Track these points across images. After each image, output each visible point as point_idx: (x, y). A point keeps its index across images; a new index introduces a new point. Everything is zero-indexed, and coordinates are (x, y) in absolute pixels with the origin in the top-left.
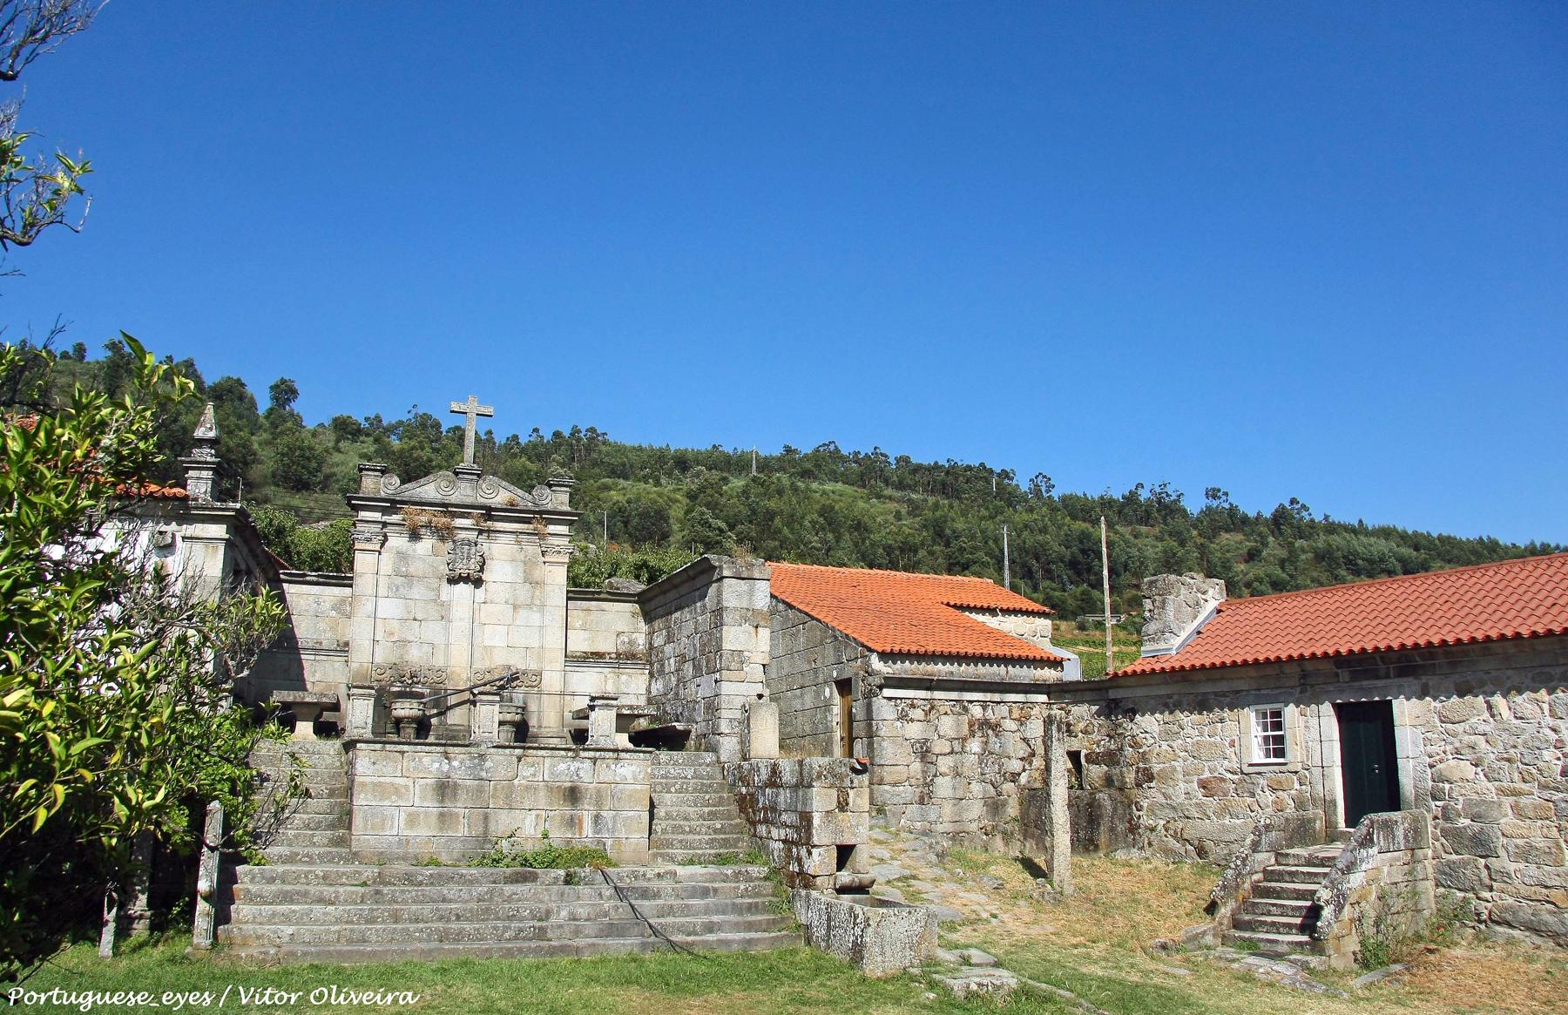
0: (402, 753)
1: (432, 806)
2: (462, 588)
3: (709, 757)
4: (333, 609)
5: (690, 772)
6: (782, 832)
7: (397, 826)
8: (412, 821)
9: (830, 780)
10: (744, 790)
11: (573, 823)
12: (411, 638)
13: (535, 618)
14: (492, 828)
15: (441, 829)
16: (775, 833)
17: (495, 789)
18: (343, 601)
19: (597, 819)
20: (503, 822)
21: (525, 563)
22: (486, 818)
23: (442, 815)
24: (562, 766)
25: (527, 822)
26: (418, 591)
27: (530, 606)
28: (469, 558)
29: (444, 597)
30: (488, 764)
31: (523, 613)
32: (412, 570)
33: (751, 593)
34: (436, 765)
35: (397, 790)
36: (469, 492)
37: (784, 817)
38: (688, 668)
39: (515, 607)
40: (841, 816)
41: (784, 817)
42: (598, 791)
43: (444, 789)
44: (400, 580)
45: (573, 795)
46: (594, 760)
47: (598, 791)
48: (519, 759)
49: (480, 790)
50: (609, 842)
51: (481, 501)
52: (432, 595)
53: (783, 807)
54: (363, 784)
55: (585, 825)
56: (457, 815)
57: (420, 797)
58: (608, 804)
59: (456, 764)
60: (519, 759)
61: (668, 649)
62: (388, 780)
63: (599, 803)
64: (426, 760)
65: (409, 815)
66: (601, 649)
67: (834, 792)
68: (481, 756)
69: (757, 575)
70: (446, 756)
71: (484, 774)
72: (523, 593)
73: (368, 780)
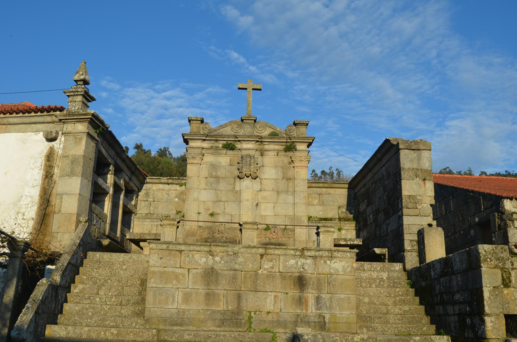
0: (181, 251)
1: (201, 288)
2: (247, 182)
3: (398, 266)
4: (176, 197)
5: (385, 275)
6: (457, 308)
7: (175, 305)
8: (187, 298)
9: (494, 262)
10: (424, 284)
11: (301, 302)
12: (219, 211)
13: (290, 199)
14: (244, 303)
15: (207, 305)
16: (450, 309)
17: (245, 277)
18: (182, 193)
19: (318, 299)
20: (251, 302)
21: (282, 168)
22: (239, 297)
23: (208, 295)
24: (292, 262)
25: (268, 300)
26: (222, 186)
27: (287, 192)
28: (250, 165)
29: (237, 188)
30: (241, 259)
31: (283, 196)
32: (219, 174)
33: (419, 158)
34: (204, 260)
35: (177, 277)
36: (250, 130)
37: (457, 297)
38: (381, 216)
39: (278, 193)
40: (506, 291)
41: (457, 297)
42: (319, 280)
43: (210, 275)
44: (212, 180)
45: (301, 282)
46: (314, 257)
47: (319, 280)
48: (262, 256)
49: (235, 278)
50: (327, 317)
51: (256, 134)
52: (230, 187)
53: (455, 289)
54: (154, 273)
55: (310, 304)
56: (219, 295)
57: (193, 283)
58: (326, 289)
59: (217, 259)
60: (262, 256)
61: (369, 210)
62: (170, 269)
63: (319, 289)
64: (197, 256)
65: (185, 294)
66: (329, 216)
67: (499, 272)
68: (235, 254)
69: (422, 148)
70: (211, 253)
71: (237, 267)
72: (282, 185)
73: (156, 269)
